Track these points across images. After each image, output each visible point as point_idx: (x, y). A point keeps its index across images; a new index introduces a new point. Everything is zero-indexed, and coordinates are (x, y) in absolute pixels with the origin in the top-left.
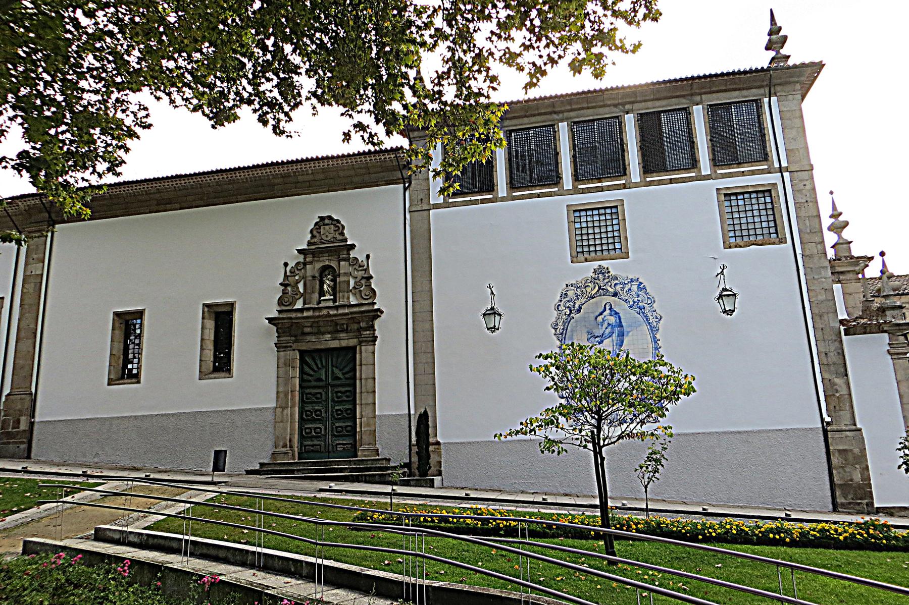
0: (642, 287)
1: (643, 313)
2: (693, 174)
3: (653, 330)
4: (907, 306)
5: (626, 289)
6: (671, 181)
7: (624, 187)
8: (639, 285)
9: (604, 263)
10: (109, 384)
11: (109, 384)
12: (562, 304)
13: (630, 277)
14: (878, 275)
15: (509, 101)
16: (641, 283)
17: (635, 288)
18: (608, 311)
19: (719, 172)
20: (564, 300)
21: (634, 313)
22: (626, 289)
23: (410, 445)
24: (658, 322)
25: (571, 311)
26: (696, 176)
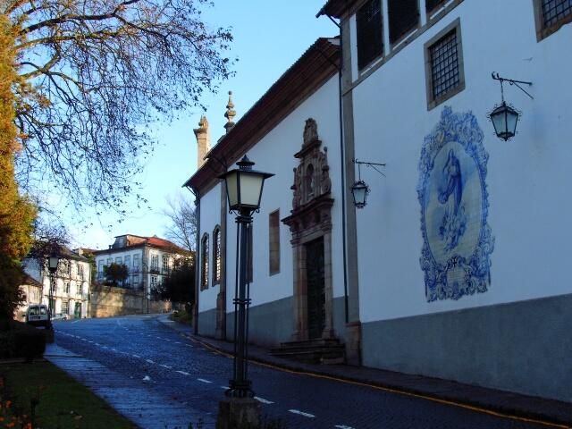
17: (469, 125)
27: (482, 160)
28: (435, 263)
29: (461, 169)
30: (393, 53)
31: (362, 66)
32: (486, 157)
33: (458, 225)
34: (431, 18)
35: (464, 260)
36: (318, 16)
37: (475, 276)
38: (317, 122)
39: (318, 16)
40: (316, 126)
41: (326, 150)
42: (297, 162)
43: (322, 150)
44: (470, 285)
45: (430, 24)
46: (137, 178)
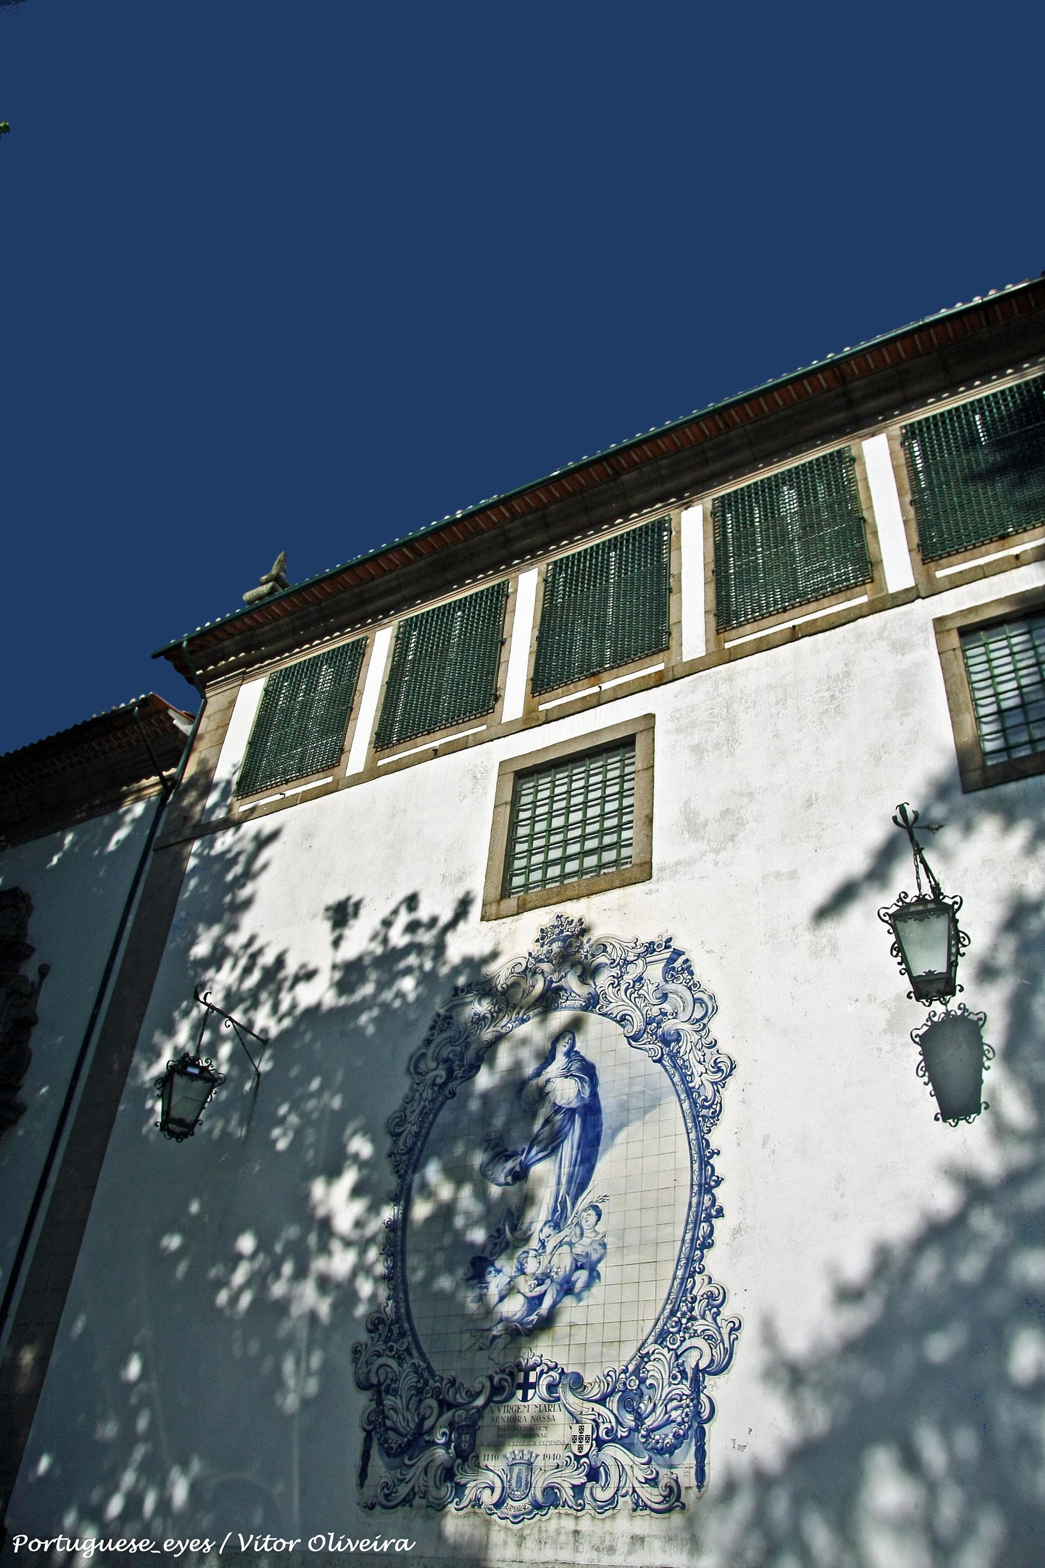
0: (677, 965)
1: (674, 1056)
2: (864, 599)
3: (702, 1114)
4: (1043, 1267)
5: (628, 978)
6: (794, 635)
7: (660, 680)
8: (671, 960)
9: (573, 910)
10: (651, 717)
11: (651, 717)
12: (430, 1052)
13: (645, 939)
14: (369, 1394)
15: (180, 678)
16: (678, 953)
17: (655, 973)
18: (560, 1061)
19: (939, 574)
20: (438, 1039)
21: (641, 1061)
22: (628, 978)
23: (692, 1185)
24: (718, 1085)
25: (450, 1072)
26: (871, 602)
27: (702, 1078)
28: (425, 1373)
29: (601, 1090)
30: (372, 773)
31: (382, 741)
32: (724, 1071)
33: (563, 1262)
34: (380, 763)
35: (577, 1383)
36: (155, 657)
37: (627, 1444)
38: (34, 901)
39: (155, 657)
40: (30, 908)
41: (44, 971)
42: (945, 1199)
43: (30, 970)
44: (593, 1475)
45: (531, 721)
46: (901, 967)
